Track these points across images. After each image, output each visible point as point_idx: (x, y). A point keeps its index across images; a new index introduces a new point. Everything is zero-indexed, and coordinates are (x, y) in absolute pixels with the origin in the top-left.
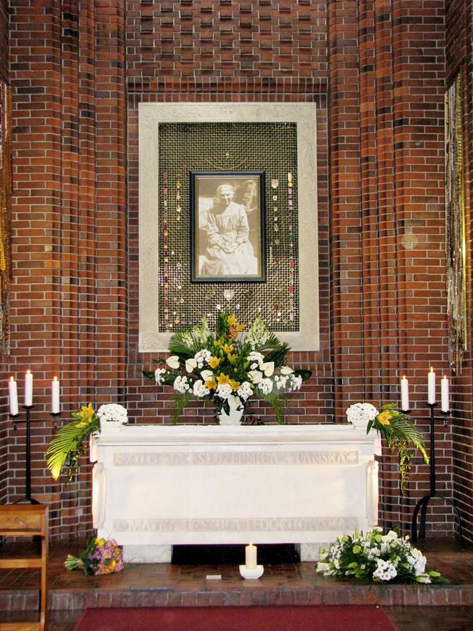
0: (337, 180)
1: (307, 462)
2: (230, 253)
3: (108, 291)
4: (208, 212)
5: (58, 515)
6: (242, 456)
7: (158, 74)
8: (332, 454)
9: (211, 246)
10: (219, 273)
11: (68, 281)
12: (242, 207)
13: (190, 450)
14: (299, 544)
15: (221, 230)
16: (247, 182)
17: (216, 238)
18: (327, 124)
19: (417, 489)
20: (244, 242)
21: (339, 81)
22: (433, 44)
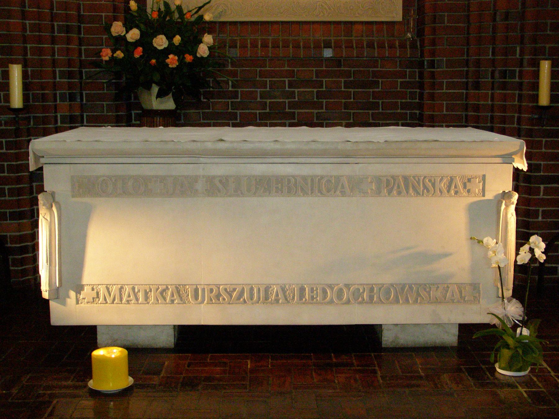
1: (399, 193)
5: (31, 249)
6: (289, 181)
8: (441, 180)
19: (540, 219)
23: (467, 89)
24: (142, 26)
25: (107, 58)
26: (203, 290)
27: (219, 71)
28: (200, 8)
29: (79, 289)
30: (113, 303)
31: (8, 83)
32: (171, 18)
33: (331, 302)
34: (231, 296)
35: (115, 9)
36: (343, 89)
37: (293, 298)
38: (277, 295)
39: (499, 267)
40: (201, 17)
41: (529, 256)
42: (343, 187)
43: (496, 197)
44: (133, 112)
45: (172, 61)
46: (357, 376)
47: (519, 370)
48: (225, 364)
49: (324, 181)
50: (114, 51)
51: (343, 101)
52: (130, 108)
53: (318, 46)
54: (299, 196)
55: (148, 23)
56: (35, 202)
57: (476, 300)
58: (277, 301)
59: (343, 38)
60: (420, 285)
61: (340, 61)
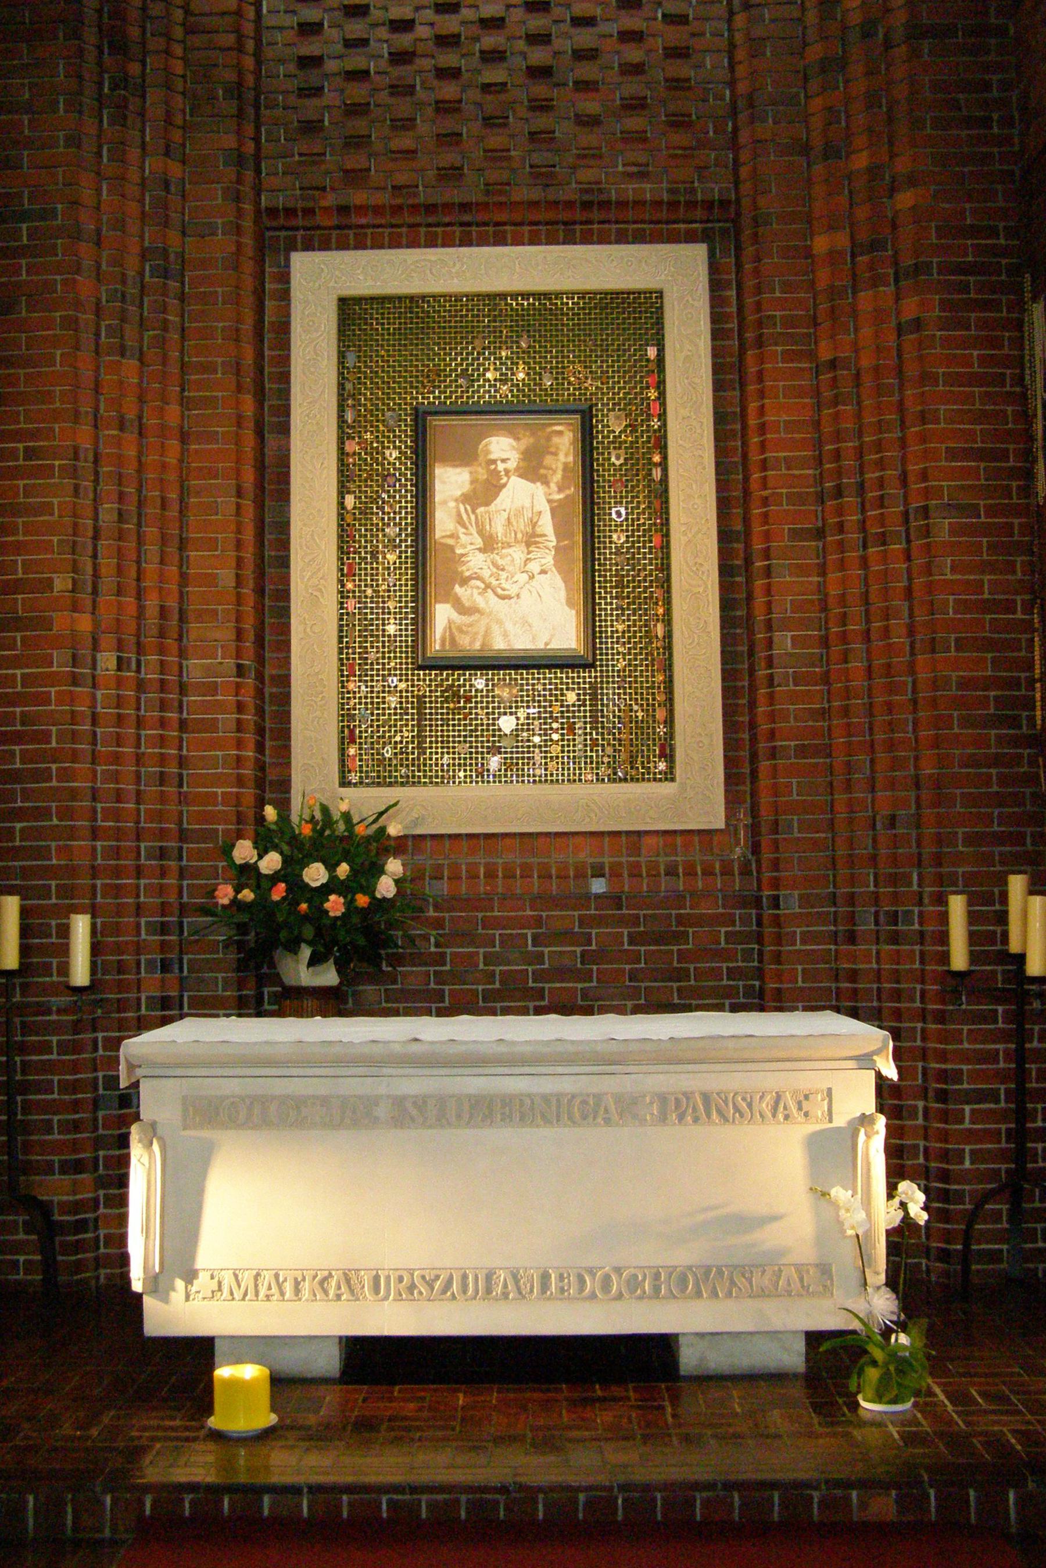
0: (763, 453)
1: (696, 1120)
2: (510, 598)
3: (213, 689)
4: (456, 500)
7: (337, 185)
8: (761, 1098)
9: (464, 581)
10: (483, 645)
11: (113, 664)
12: (539, 489)
13: (381, 1088)
14: (677, 1335)
15: (489, 545)
16: (549, 429)
17: (476, 562)
18: (734, 293)
19: (967, 1164)
20: (543, 572)
21: (760, 221)
22: (987, 86)
23: (836, 944)
24: (285, 848)
25: (226, 901)
26: (388, 1278)
27: (413, 919)
28: (381, 814)
29: (190, 1276)
30: (243, 1299)
31: (68, 945)
32: (333, 831)
33: (593, 1296)
34: (432, 1289)
35: (240, 819)
36: (626, 947)
37: (532, 1291)
38: (505, 1286)
39: (857, 1236)
40: (382, 830)
41: (901, 1214)
42: (606, 1111)
43: (850, 1122)
44: (266, 990)
45: (335, 905)
46: (634, 1415)
47: (894, 1401)
48: (423, 1399)
49: (578, 1100)
50: (238, 891)
51: (627, 967)
52: (261, 981)
53: (581, 875)
54: (538, 1126)
55: (294, 840)
56: (124, 1142)
57: (827, 1291)
58: (505, 1295)
59: (624, 859)
60: (736, 1267)
61: (620, 898)
